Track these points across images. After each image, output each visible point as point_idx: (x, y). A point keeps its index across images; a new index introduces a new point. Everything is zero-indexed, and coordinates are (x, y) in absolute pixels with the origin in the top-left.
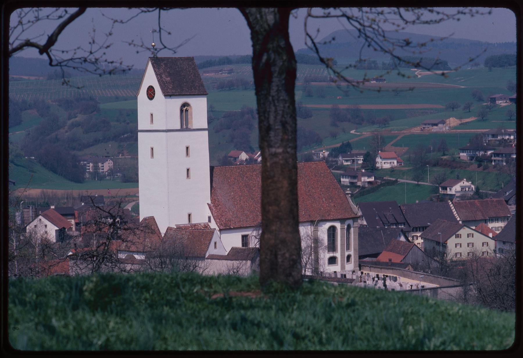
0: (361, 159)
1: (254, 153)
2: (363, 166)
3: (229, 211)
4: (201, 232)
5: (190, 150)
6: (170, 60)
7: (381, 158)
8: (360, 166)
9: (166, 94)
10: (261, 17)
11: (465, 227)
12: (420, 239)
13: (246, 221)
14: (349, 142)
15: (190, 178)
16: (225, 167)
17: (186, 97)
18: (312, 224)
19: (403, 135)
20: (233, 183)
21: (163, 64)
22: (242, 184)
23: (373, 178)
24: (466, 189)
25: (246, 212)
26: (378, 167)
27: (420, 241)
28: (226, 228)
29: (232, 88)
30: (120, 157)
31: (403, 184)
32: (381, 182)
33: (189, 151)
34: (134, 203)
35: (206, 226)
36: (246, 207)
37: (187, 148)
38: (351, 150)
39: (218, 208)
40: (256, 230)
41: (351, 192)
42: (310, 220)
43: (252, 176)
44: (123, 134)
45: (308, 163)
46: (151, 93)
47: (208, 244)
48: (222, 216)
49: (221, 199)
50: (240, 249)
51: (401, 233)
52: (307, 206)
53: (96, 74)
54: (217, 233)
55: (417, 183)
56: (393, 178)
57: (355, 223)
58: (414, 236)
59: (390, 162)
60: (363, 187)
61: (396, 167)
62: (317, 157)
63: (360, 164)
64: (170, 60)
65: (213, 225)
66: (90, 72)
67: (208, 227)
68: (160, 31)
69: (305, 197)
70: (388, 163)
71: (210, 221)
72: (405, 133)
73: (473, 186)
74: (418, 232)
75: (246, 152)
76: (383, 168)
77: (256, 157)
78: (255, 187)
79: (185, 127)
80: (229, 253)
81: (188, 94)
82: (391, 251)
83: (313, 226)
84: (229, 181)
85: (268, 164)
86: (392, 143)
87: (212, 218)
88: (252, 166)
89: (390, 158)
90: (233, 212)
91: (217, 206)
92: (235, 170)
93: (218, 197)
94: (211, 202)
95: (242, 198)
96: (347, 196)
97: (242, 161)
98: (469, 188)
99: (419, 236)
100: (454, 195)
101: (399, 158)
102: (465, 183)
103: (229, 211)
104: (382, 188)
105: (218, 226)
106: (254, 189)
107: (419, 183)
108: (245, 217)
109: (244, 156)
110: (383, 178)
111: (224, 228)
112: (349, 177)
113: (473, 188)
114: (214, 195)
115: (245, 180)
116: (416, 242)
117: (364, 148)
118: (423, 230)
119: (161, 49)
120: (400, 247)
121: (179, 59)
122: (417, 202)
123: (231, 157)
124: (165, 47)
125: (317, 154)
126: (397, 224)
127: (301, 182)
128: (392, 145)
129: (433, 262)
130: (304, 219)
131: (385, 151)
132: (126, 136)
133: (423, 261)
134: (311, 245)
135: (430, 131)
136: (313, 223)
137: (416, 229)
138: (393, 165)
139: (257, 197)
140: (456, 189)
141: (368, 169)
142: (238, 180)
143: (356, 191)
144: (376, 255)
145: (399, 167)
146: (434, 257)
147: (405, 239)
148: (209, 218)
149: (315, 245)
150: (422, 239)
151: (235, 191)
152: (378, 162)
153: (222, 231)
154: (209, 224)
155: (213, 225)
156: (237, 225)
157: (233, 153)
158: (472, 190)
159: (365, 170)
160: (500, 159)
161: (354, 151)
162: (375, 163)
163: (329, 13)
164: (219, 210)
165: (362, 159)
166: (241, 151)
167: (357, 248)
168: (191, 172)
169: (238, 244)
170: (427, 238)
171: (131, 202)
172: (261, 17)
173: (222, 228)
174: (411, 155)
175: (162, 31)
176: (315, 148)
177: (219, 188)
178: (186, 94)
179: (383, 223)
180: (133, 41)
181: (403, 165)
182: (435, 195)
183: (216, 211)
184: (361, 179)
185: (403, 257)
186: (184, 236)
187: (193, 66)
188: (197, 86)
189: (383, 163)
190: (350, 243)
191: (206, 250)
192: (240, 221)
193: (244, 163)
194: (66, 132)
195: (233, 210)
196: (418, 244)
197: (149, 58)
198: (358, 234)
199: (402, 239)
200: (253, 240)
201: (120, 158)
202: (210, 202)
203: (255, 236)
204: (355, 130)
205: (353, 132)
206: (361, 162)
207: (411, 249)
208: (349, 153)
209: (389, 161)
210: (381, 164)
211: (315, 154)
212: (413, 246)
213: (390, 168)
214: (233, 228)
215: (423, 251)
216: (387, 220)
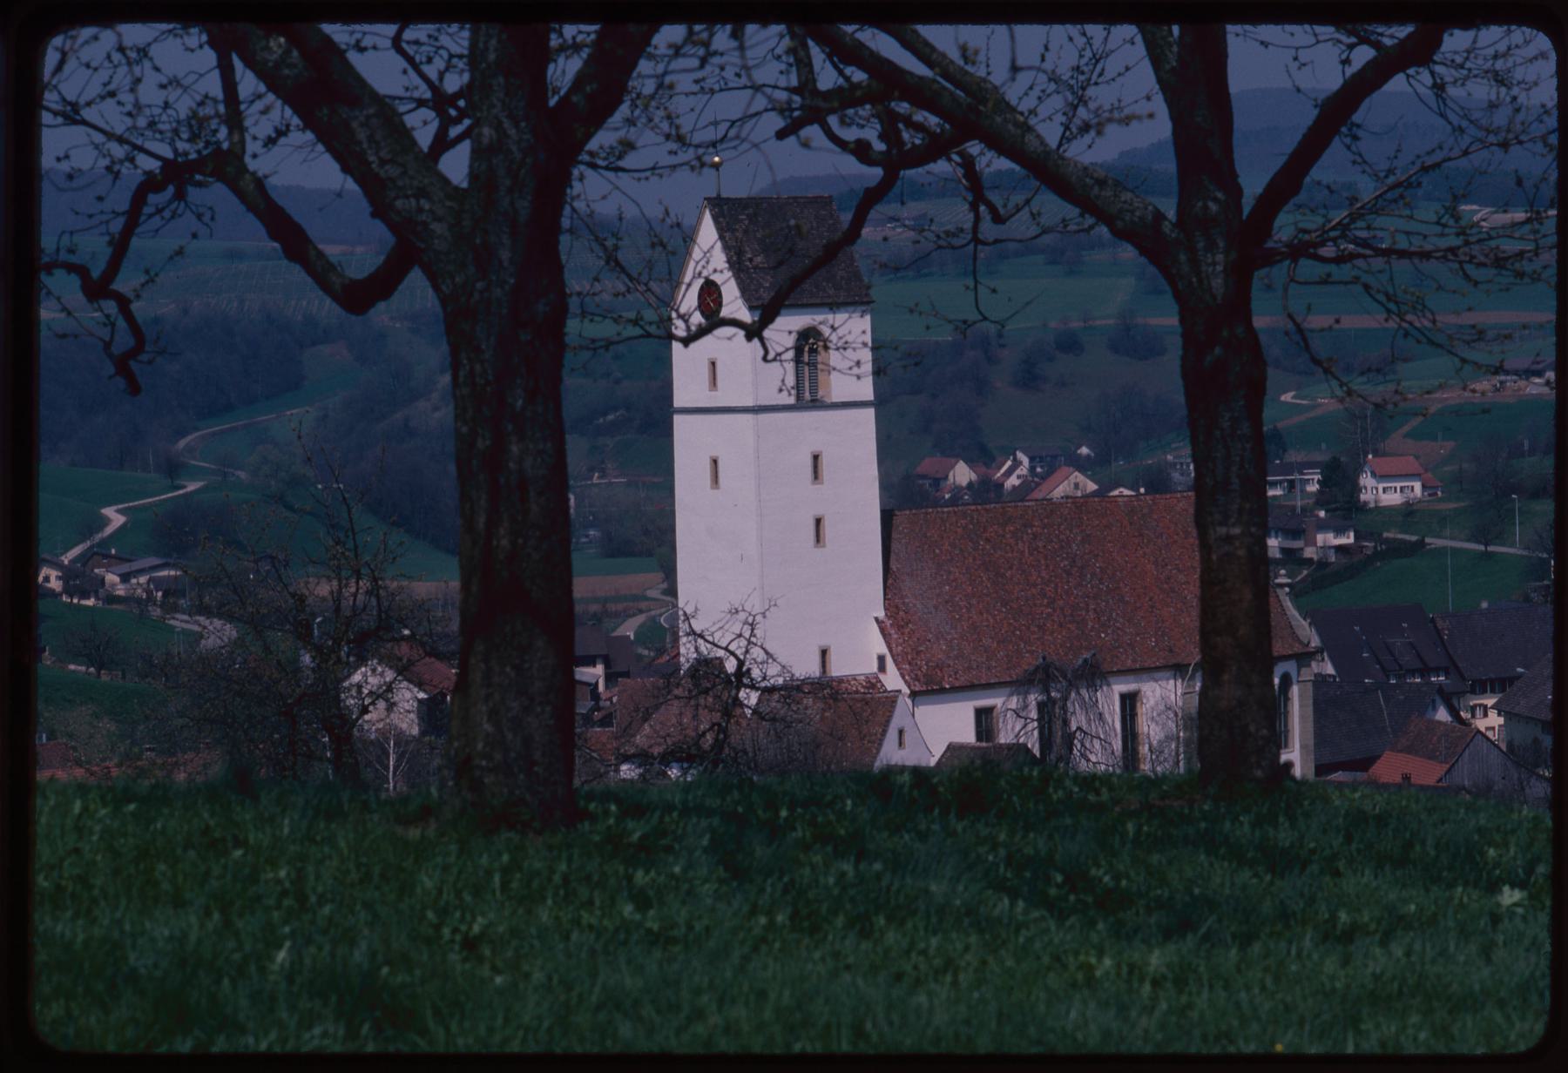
0: (1313, 480)
1: (994, 465)
2: (1321, 500)
3: (938, 639)
5: (825, 462)
6: (765, 205)
7: (1374, 474)
8: (1311, 501)
9: (755, 304)
10: (1200, 281)
12: (1493, 714)
13: (989, 668)
14: (1275, 427)
15: (824, 546)
16: (923, 510)
17: (809, 310)
18: (1178, 674)
19: (1440, 406)
20: (949, 557)
21: (744, 217)
22: (974, 559)
23: (1352, 534)
25: (987, 641)
26: (1366, 503)
27: (1495, 720)
28: (929, 688)
29: (925, 271)
30: (595, 480)
31: (1441, 552)
32: (1375, 547)
33: (819, 465)
34: (641, 619)
35: (873, 683)
36: (987, 626)
37: (816, 458)
38: (1285, 451)
39: (907, 631)
40: (1018, 694)
41: (1289, 581)
42: (1173, 661)
43: (1003, 536)
44: (605, 414)
45: (1164, 496)
47: (879, 736)
48: (918, 653)
49: (915, 605)
50: (973, 748)
51: (1438, 700)
52: (1163, 621)
53: (851, 375)
54: (904, 702)
55: (1482, 548)
56: (1412, 534)
57: (1304, 670)
58: (1476, 706)
59: (1402, 488)
60: (1322, 564)
61: (1420, 501)
62: (1182, 475)
63: (1312, 493)
64: (765, 205)
65: (893, 680)
66: (839, 371)
67: (879, 685)
68: (976, 287)
69: (1156, 597)
70: (1396, 491)
71: (882, 667)
72: (1446, 399)
74: (1488, 694)
75: (970, 462)
76: (1381, 505)
77: (999, 475)
78: (1011, 568)
79: (807, 396)
80: (940, 759)
81: (818, 301)
82: (1409, 753)
83: (1183, 680)
84: (937, 551)
85: (1214, 557)
86: (1406, 428)
87: (889, 661)
88: (1003, 508)
89: (1401, 476)
90: (951, 641)
91: (902, 627)
92: (954, 519)
93: (907, 600)
94: (886, 615)
95: (974, 601)
96: (1279, 591)
97: (957, 491)
99: (1492, 708)
101: (1429, 475)
103: (938, 639)
104: (1379, 564)
105: (906, 682)
106: (1008, 574)
107: (1491, 548)
108: (985, 655)
109: (962, 474)
110: (1381, 535)
111: (924, 688)
112: (1280, 534)
114: (895, 594)
115: (983, 550)
116: (1481, 724)
117: (1324, 446)
118: (1503, 690)
119: (975, 323)
120: (1435, 738)
121: (791, 201)
122: (1484, 605)
123: (924, 477)
124: (985, 319)
125: (1182, 464)
126: (1425, 671)
127: (1145, 553)
128: (1406, 436)
129: (1533, 780)
130: (1154, 659)
131: (1384, 455)
132: (611, 417)
133: (1503, 778)
134: (1178, 733)
135: (1521, 392)
136: (1181, 671)
137: (1480, 687)
138: (1412, 496)
139: (1018, 598)
141: (1336, 509)
142: (961, 550)
143: (1302, 576)
144: (1364, 764)
145: (1428, 501)
146: (1537, 766)
147: (1451, 715)
148: (881, 659)
149: (1188, 734)
150: (1499, 715)
151: (955, 580)
152: (1366, 488)
153: (917, 699)
154: (881, 677)
155: (893, 680)
156: (963, 679)
157: (928, 465)
159: (1327, 511)
161: (1293, 456)
162: (1357, 489)
163: (1329, 275)
164: (910, 638)
165: (1319, 480)
166: (953, 460)
167: (1311, 742)
168: (828, 530)
169: (968, 735)
170: (1516, 710)
171: (634, 615)
172: (1200, 281)
173: (917, 689)
174: (1465, 466)
175: (979, 286)
176: (1176, 449)
177: (908, 574)
179: (1383, 668)
180: (917, 305)
181: (1439, 493)
182: (1538, 584)
183: (901, 641)
184: (1315, 538)
185: (1445, 769)
187: (831, 222)
188: (842, 278)
189: (1381, 490)
190: (1290, 727)
191: (875, 751)
192: (970, 668)
193: (966, 494)
194: (436, 409)
195: (949, 637)
196: (1487, 729)
197: (705, 199)
198: (1311, 702)
199: (1442, 715)
200: (1010, 721)
201: (596, 484)
202: (881, 614)
203: (1014, 710)
204: (1292, 393)
205: (1287, 397)
206: (1313, 488)
207: (1468, 745)
208: (1278, 462)
209: (1398, 485)
210: (1374, 492)
211: (1175, 464)
212: (1473, 737)
213: (1402, 504)
214: (951, 688)
215: (1505, 749)
216: (1396, 660)
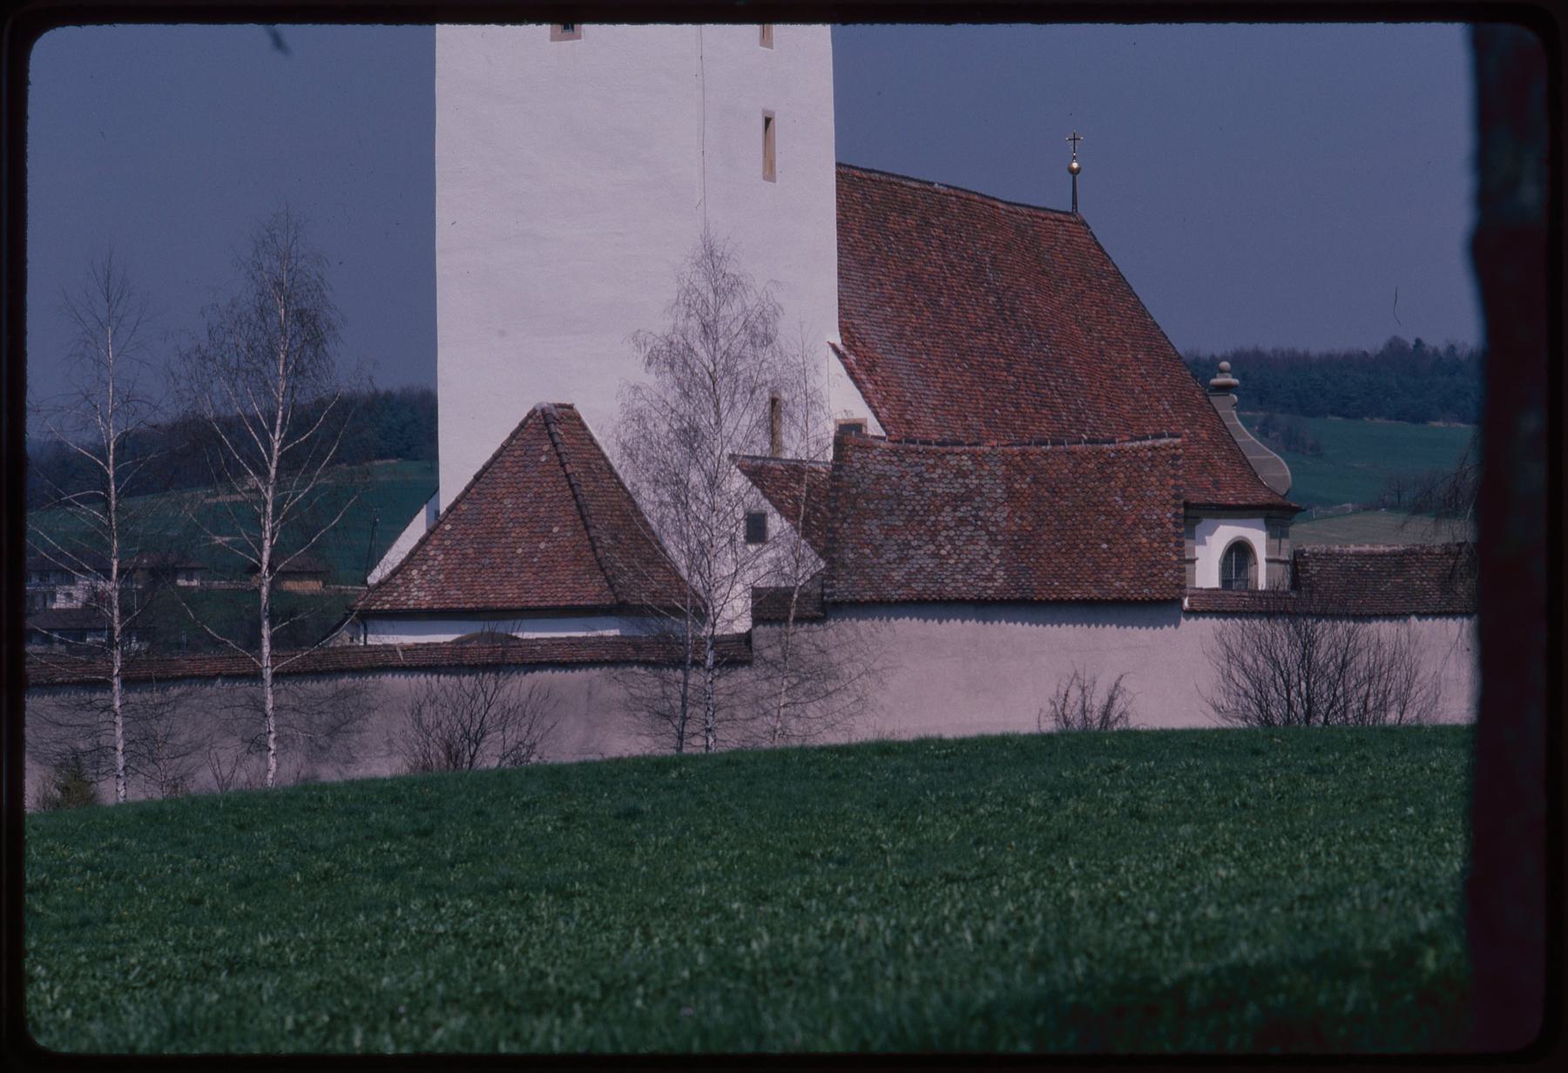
202: (838, 341)
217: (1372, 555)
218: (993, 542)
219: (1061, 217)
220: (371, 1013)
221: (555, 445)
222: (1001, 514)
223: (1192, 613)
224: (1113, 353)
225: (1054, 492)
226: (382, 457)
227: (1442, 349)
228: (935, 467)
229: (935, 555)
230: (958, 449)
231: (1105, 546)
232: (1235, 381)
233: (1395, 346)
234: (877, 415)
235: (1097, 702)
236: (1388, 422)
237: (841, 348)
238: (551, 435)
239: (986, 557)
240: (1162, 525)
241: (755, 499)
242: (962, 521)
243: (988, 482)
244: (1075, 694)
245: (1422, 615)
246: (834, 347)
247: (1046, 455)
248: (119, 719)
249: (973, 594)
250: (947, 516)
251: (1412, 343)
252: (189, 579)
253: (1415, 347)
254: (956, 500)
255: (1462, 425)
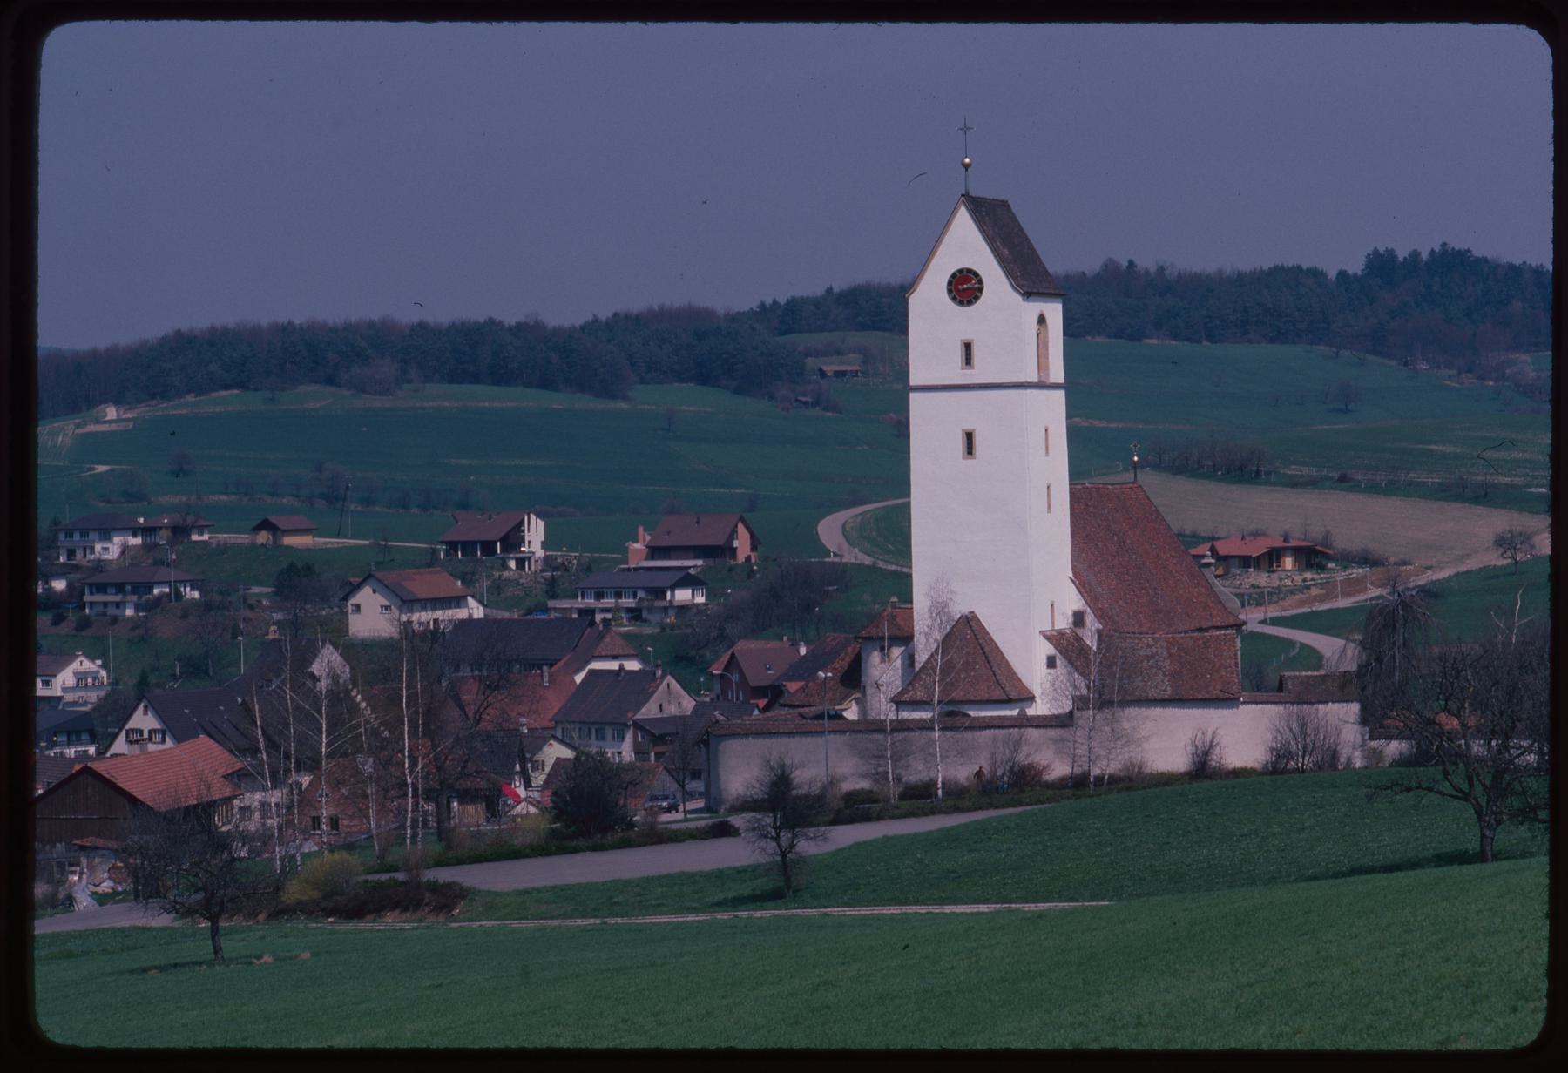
4: (1198, 639)
11: (552, 742)
24: (86, 681)
46: (965, 288)
73: (103, 673)
98: (94, 679)
100: (60, 698)
102: (83, 664)
113: (103, 678)
140: (64, 683)
154: (1080, 632)
158: (102, 683)
160: (118, 598)
178: (1041, 290)
186: (1154, 649)
202: (1071, 575)
217: (1311, 676)
218: (1165, 675)
219: (1131, 485)
220: (57, 876)
221: (973, 631)
222: (1167, 663)
223: (1243, 703)
224: (1162, 555)
225: (1186, 653)
226: (226, 387)
227: (1153, 269)
228: (1138, 644)
229: (1142, 681)
230: (1147, 636)
231: (1209, 676)
232: (1213, 561)
233: (1111, 268)
234: (1090, 607)
235: (1208, 739)
236: (1108, 340)
237: (1073, 578)
238: (971, 627)
239: (1163, 681)
240: (1230, 667)
241: (1050, 650)
242: (1152, 667)
243: (1159, 649)
244: (1200, 736)
245: (1333, 702)
246: (1071, 578)
247: (1182, 638)
248: (890, 762)
249: (1160, 697)
250: (1145, 664)
251: (1125, 264)
252: (201, 533)
253: (1127, 267)
254: (1149, 658)
255: (1174, 343)
